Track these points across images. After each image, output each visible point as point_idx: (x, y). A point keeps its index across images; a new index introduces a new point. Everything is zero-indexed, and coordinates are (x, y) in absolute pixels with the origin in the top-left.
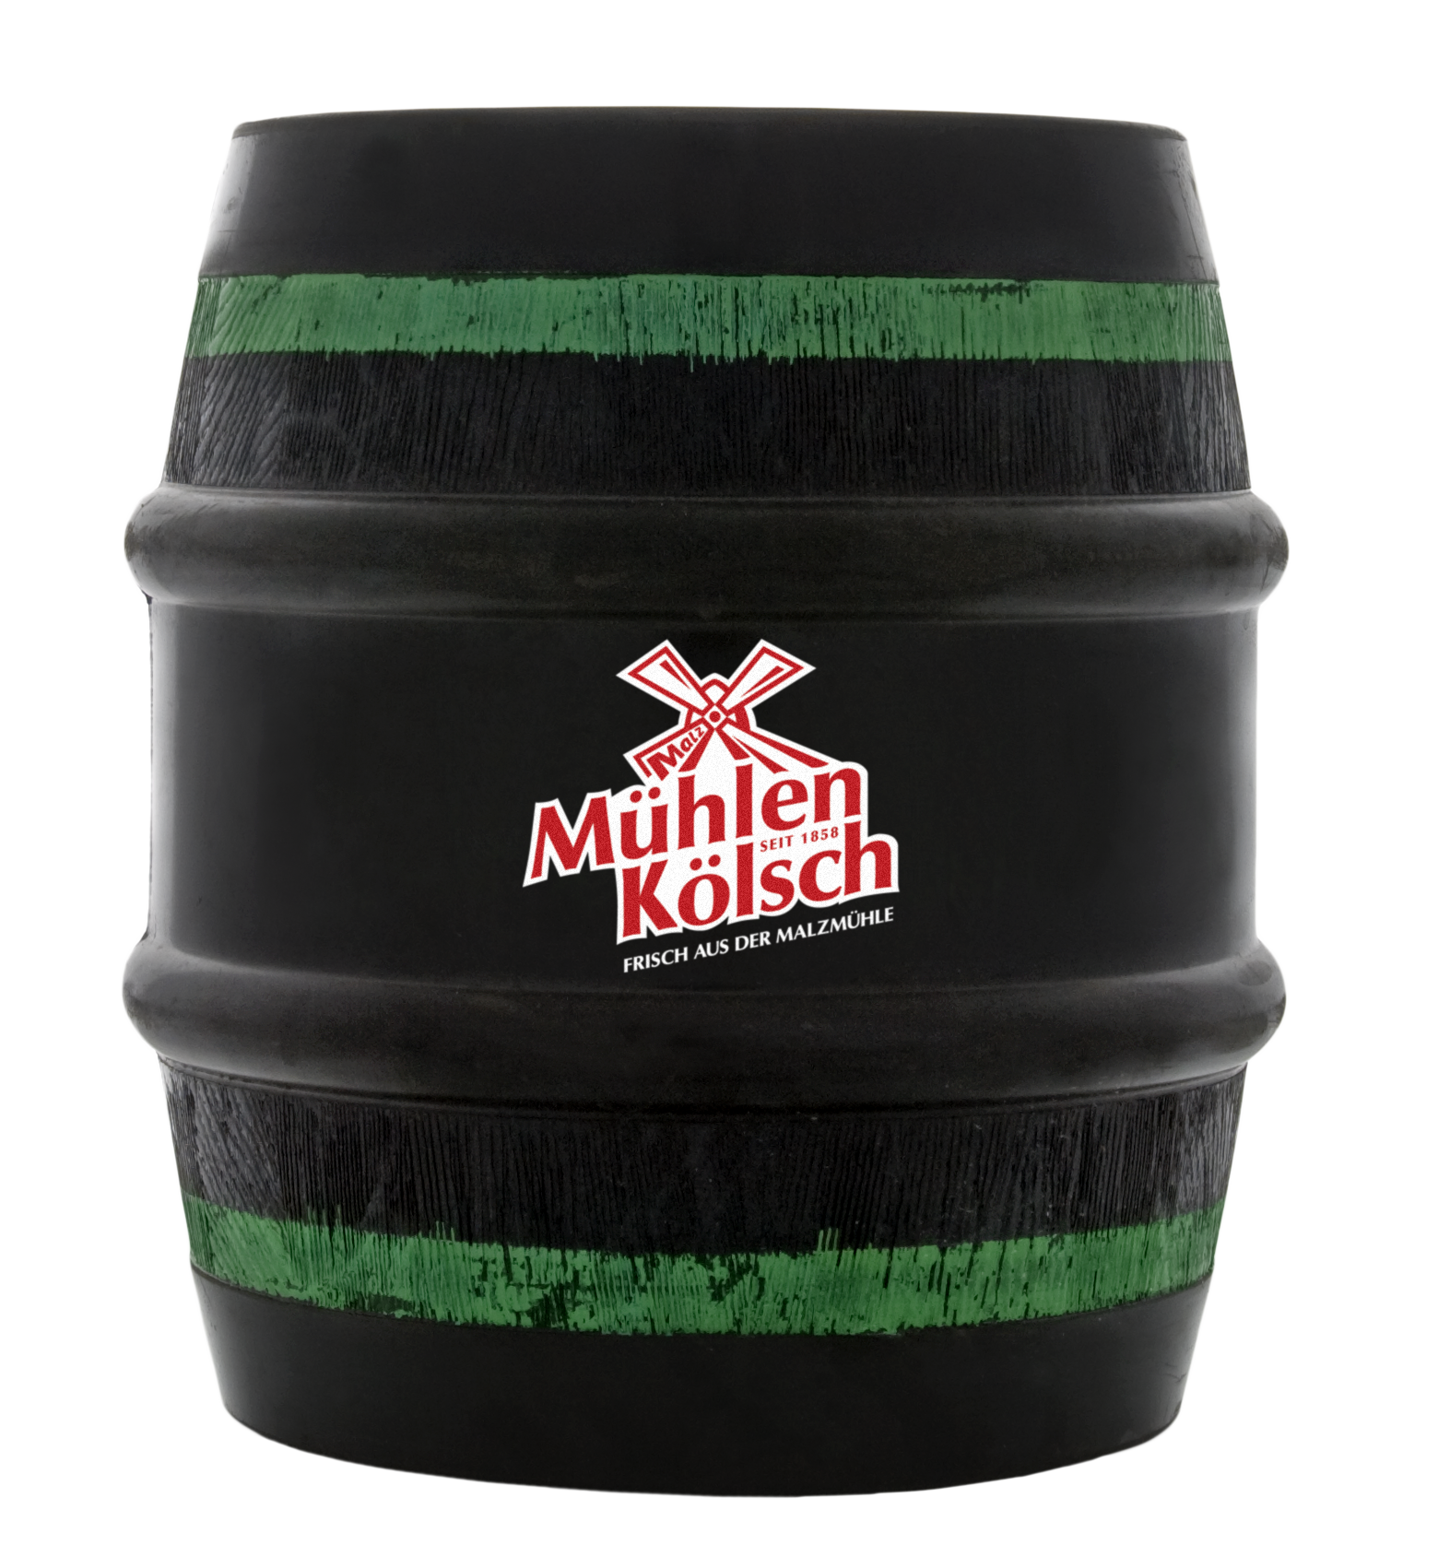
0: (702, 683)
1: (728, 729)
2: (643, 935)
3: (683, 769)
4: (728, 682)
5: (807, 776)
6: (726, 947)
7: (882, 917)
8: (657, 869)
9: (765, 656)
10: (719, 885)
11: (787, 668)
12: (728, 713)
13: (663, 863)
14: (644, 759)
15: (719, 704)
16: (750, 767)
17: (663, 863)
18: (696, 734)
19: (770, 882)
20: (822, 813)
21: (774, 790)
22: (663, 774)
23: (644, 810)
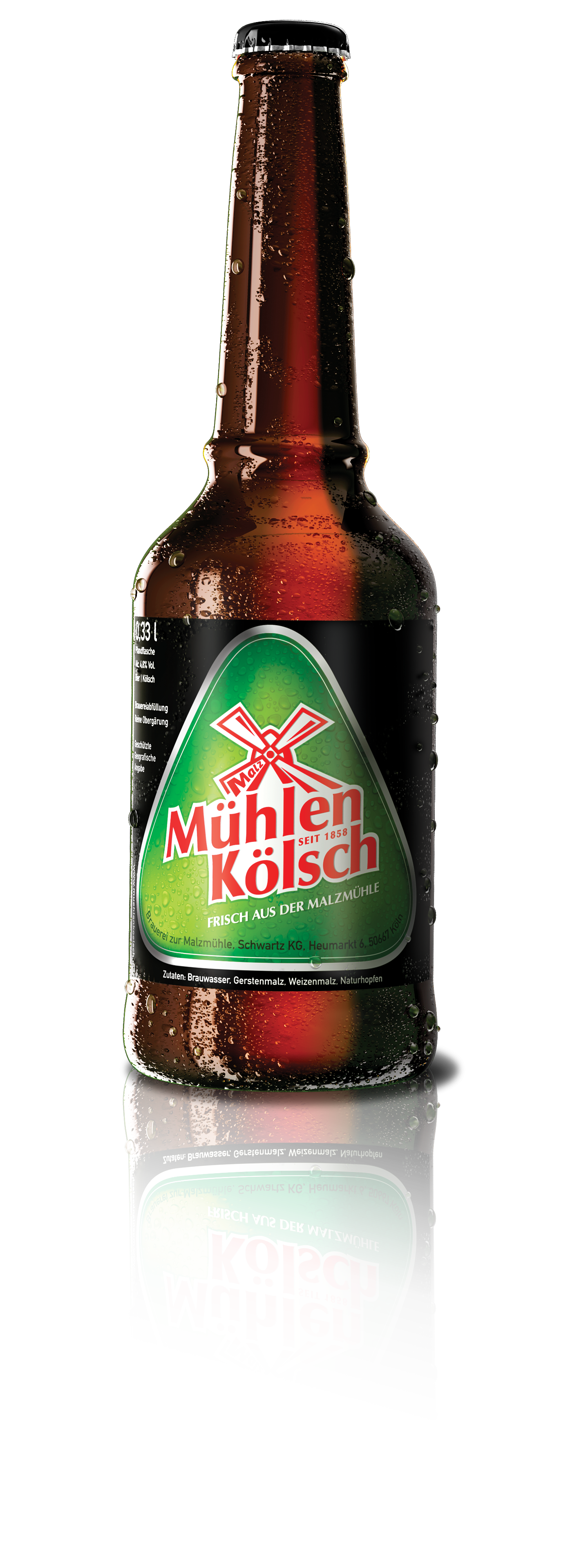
0: (262, 731)
1: (280, 764)
2: (224, 900)
3: (249, 790)
4: (279, 732)
6: (274, 912)
7: (373, 890)
8: (233, 856)
9: (304, 714)
10: (272, 868)
11: (317, 722)
12: (278, 752)
13: (237, 852)
15: (273, 746)
16: (293, 788)
17: (237, 852)
18: (258, 766)
19: (305, 866)
20: (338, 820)
21: (309, 804)
22: (237, 792)
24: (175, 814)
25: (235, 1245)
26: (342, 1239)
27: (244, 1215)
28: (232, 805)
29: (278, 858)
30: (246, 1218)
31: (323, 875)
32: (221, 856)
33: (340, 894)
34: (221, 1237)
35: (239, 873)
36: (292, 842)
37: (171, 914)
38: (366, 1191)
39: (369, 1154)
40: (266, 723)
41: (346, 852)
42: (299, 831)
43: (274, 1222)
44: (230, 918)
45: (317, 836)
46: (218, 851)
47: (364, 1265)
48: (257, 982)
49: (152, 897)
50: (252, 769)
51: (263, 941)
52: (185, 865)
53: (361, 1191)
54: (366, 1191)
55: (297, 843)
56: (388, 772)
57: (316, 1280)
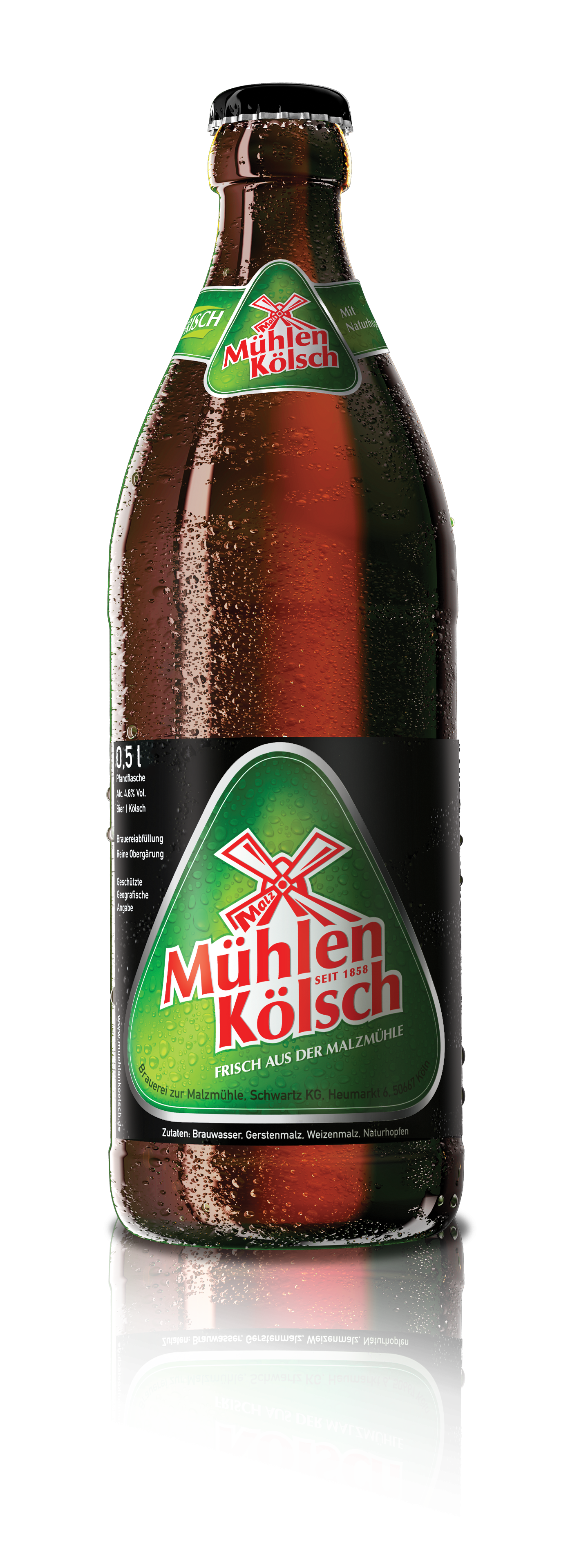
0: (273, 860)
1: (293, 894)
2: (233, 1046)
3: (259, 924)
4: (292, 859)
5: (310, 331)
6: (289, 1058)
7: (397, 1033)
8: (243, 998)
9: (318, 840)
10: (286, 1008)
11: (333, 849)
12: (291, 881)
13: (247, 993)
14: (233, 916)
16: (308, 921)
17: (247, 993)
18: (269, 898)
19: (323, 1007)
20: (357, 955)
21: (325, 938)
22: (246, 927)
23: (233, 953)
24: (173, 955)
25: (246, 1439)
26: (363, 1436)
27: (256, 1407)
28: (240, 941)
29: (293, 999)
30: (259, 1410)
31: (342, 1016)
32: (229, 998)
33: (361, 1038)
34: (230, 1430)
35: (250, 1016)
36: (309, 980)
37: (171, 1065)
38: (391, 1383)
39: (394, 1341)
40: (277, 850)
41: (367, 991)
42: (316, 969)
43: (289, 1415)
44: (240, 1066)
45: (335, 974)
46: (225, 993)
47: (387, 1464)
48: (272, 1136)
49: (145, 1048)
50: (262, 902)
51: (277, 1091)
52: (187, 1010)
53: (385, 1383)
54: (391, 1383)
55: (313, 982)
56: (411, 905)
57: (334, 1481)
